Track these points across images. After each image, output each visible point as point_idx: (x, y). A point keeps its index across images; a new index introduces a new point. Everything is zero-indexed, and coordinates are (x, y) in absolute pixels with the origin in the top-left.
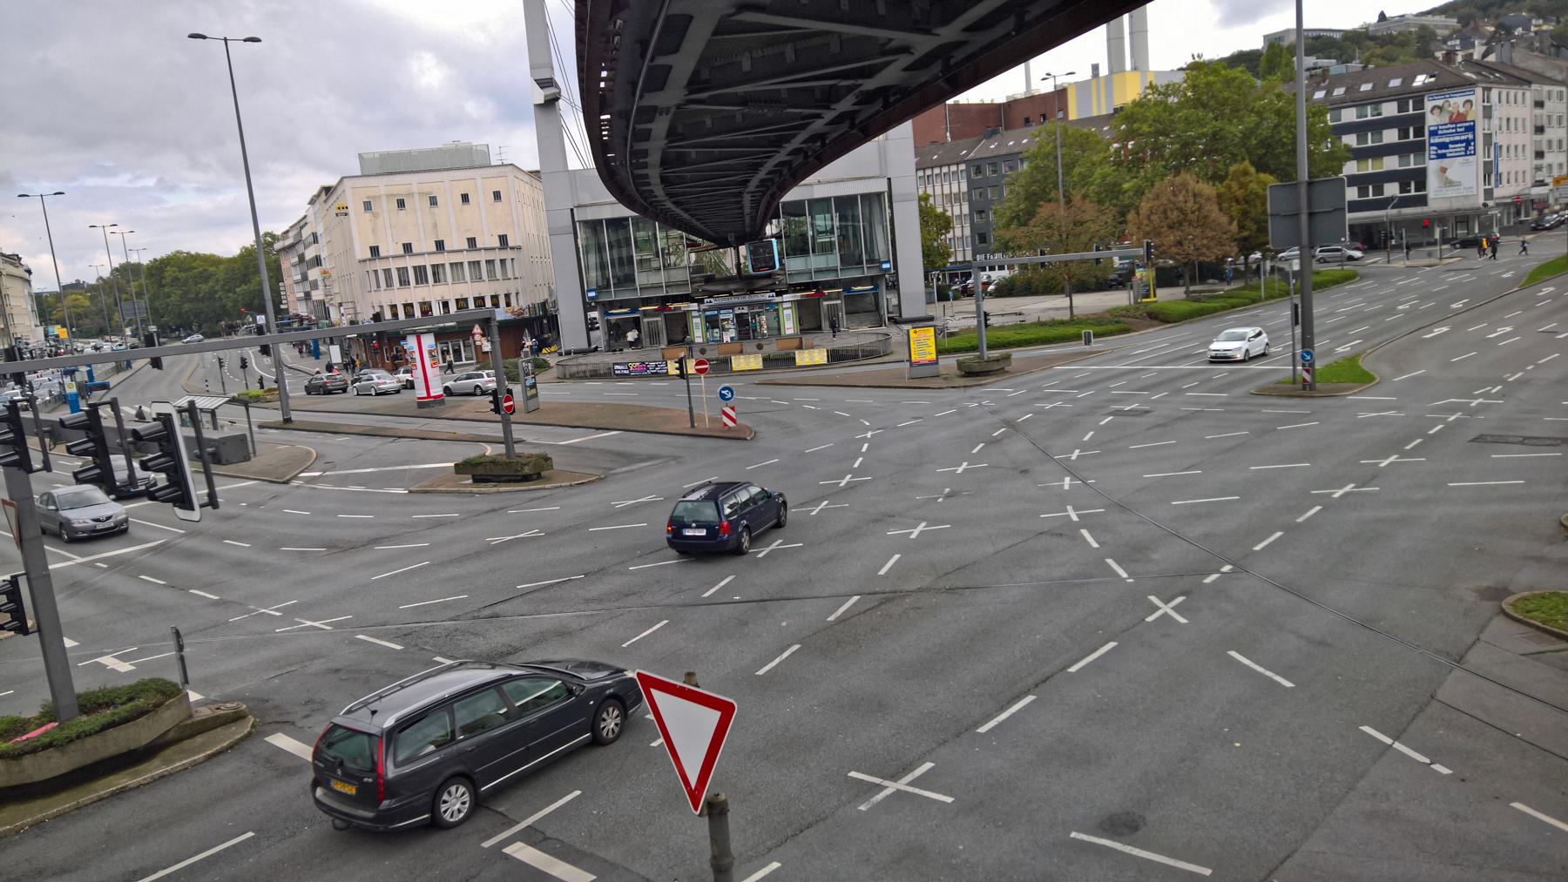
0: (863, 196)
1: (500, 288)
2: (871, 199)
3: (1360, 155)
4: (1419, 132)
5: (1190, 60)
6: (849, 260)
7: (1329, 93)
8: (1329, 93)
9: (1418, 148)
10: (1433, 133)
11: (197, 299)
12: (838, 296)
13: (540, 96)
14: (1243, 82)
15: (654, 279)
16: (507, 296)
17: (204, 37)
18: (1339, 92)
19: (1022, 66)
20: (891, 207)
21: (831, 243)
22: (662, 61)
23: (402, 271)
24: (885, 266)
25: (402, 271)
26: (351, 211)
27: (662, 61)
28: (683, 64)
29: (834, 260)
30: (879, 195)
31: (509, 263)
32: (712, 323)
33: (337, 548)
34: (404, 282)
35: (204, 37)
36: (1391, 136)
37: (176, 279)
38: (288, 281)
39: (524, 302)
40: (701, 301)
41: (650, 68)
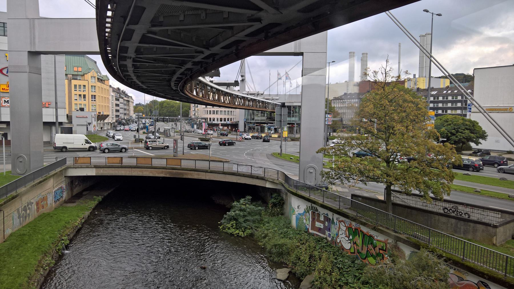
1: (230, 117)
2: (295, 107)
3: (451, 109)
4: (466, 105)
9: (465, 109)
10: (469, 105)
11: (170, 112)
14: (135, 82)
15: (258, 118)
16: (231, 119)
18: (449, 92)
19: (239, 62)
22: (132, 27)
23: (210, 111)
25: (210, 111)
27: (132, 27)
28: (140, 30)
32: (269, 129)
34: (210, 113)
36: (459, 105)
37: (166, 106)
38: (191, 110)
39: (234, 121)
40: (267, 124)
41: (126, 29)
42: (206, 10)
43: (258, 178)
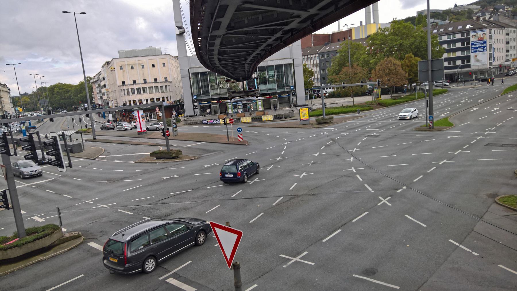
0: (285, 65)
1: (165, 95)
2: (287, 66)
3: (448, 51)
4: (468, 44)
5: (392, 20)
6: (280, 86)
7: (438, 31)
8: (438, 31)
9: (468, 49)
10: (473, 44)
11: (65, 99)
12: (276, 98)
13: (178, 32)
15: (216, 92)
16: (167, 98)
17: (67, 12)
18: (442, 30)
20: (294, 68)
21: (274, 80)
22: (218, 20)
23: (133, 90)
24: (292, 88)
25: (133, 90)
26: (116, 70)
27: (218, 20)
28: (225, 21)
29: (275, 86)
30: (290, 64)
31: (168, 87)
32: (235, 107)
33: (111, 181)
34: (133, 93)
35: (67, 12)
36: (459, 45)
37: (58, 92)
38: (95, 93)
39: (173, 100)
40: (231, 99)
41: (214, 23)
42: (277, 11)
43: (350, 107)
